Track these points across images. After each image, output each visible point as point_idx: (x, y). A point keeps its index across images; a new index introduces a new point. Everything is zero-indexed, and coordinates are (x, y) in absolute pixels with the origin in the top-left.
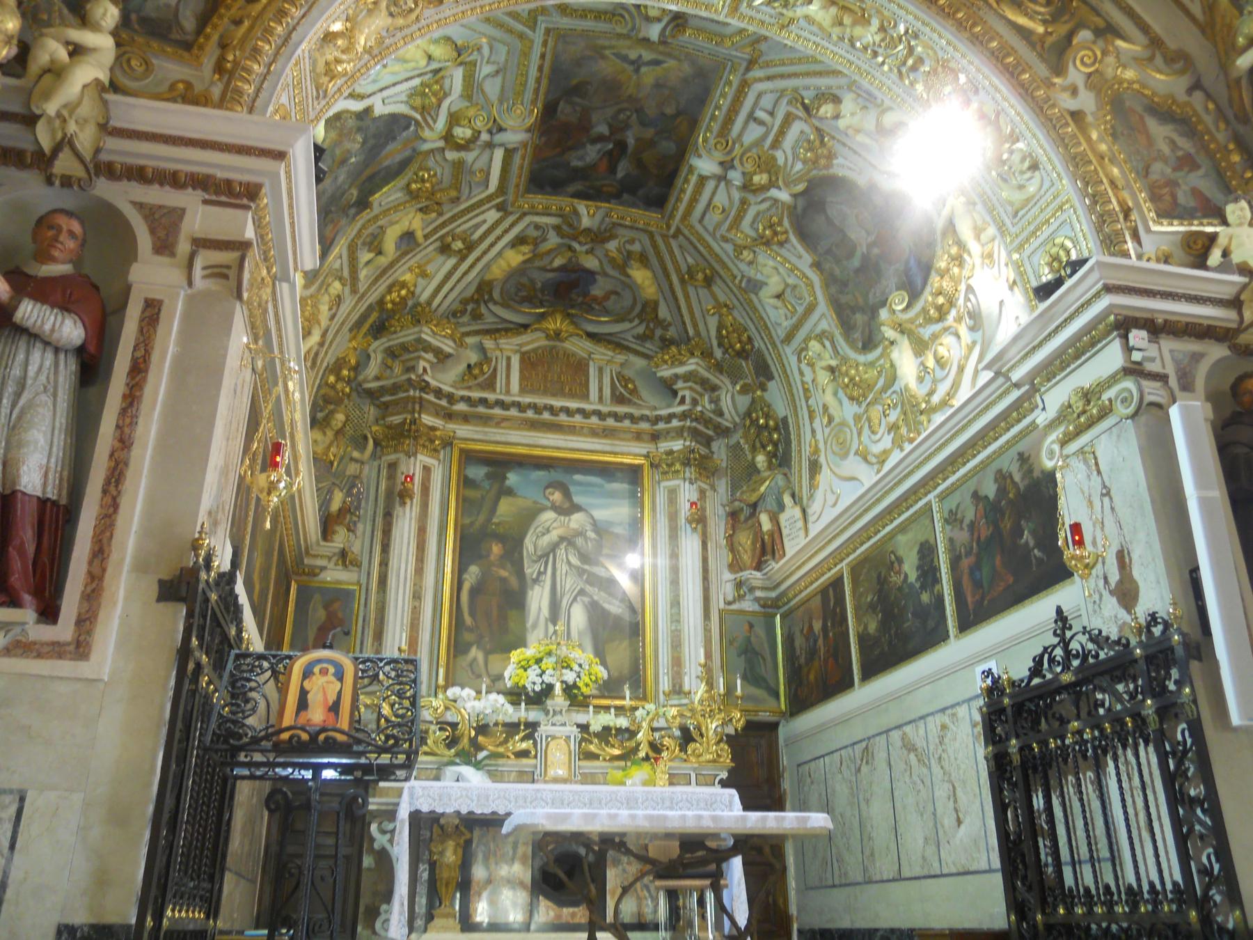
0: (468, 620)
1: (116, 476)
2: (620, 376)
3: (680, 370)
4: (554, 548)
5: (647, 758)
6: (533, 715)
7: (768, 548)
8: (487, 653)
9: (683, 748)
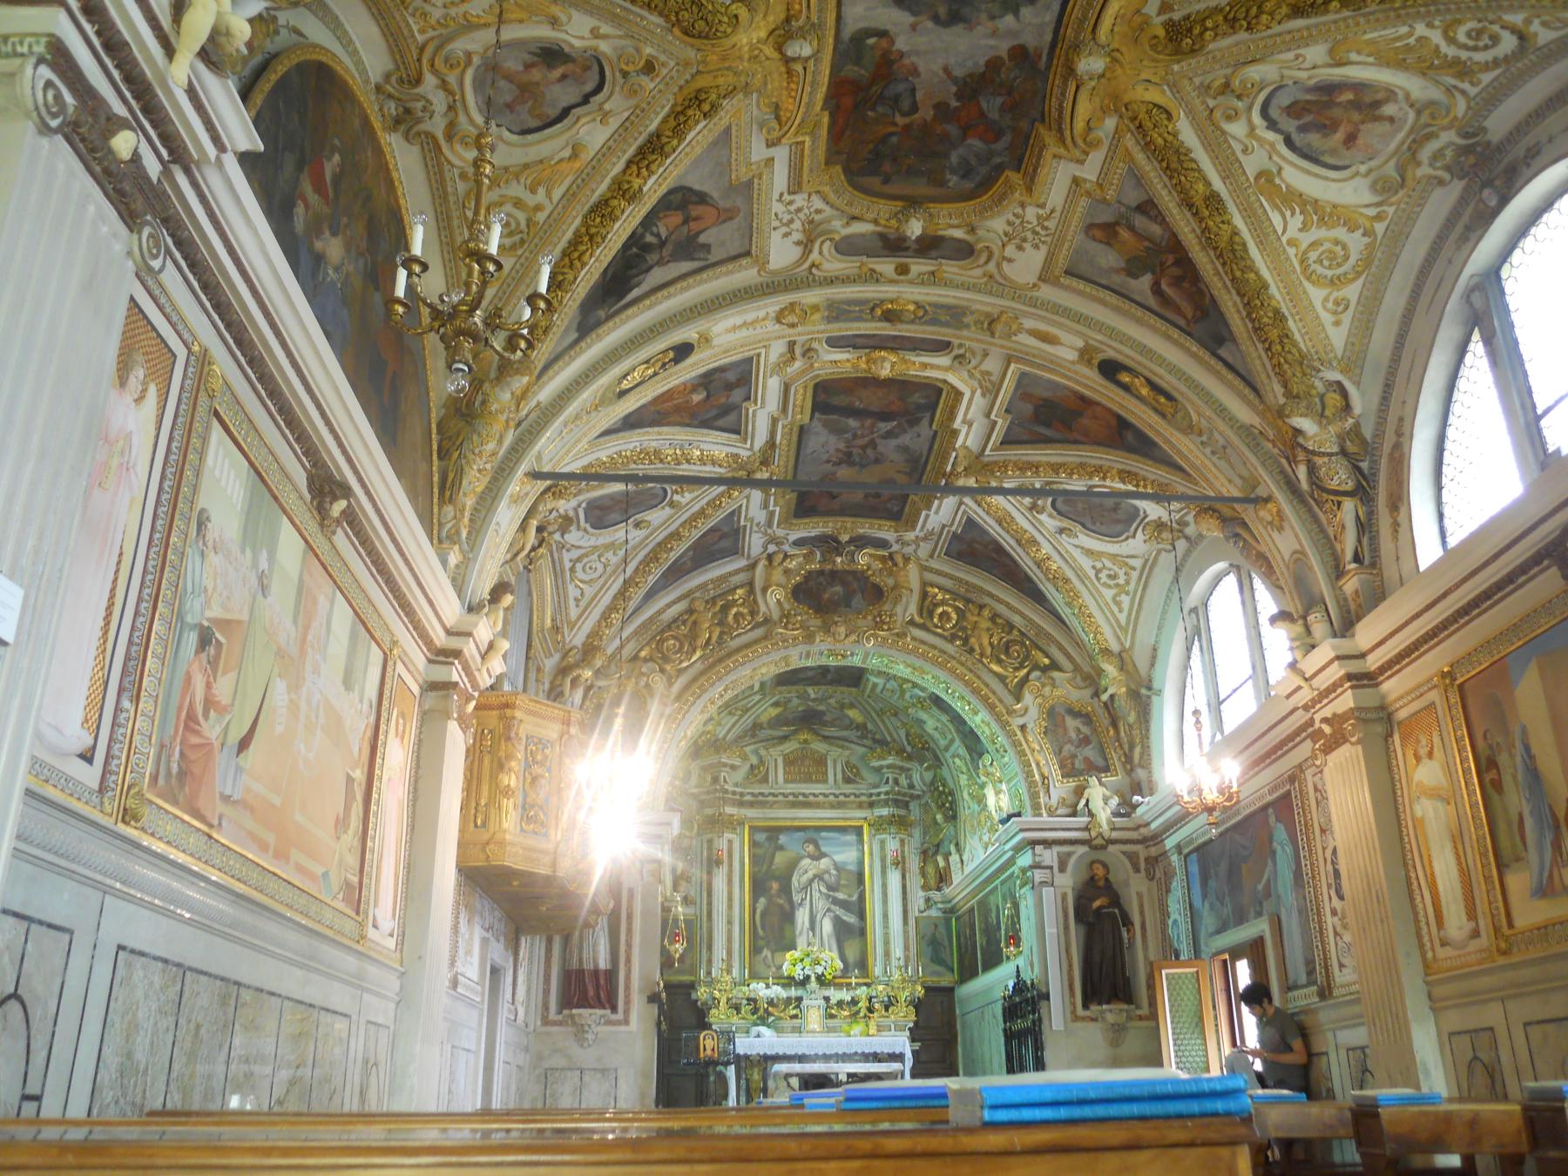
0: (761, 932)
1: (628, 961)
2: (847, 763)
3: (884, 763)
4: (811, 881)
5: (865, 1016)
6: (800, 992)
7: (943, 878)
8: (773, 952)
9: (887, 1009)
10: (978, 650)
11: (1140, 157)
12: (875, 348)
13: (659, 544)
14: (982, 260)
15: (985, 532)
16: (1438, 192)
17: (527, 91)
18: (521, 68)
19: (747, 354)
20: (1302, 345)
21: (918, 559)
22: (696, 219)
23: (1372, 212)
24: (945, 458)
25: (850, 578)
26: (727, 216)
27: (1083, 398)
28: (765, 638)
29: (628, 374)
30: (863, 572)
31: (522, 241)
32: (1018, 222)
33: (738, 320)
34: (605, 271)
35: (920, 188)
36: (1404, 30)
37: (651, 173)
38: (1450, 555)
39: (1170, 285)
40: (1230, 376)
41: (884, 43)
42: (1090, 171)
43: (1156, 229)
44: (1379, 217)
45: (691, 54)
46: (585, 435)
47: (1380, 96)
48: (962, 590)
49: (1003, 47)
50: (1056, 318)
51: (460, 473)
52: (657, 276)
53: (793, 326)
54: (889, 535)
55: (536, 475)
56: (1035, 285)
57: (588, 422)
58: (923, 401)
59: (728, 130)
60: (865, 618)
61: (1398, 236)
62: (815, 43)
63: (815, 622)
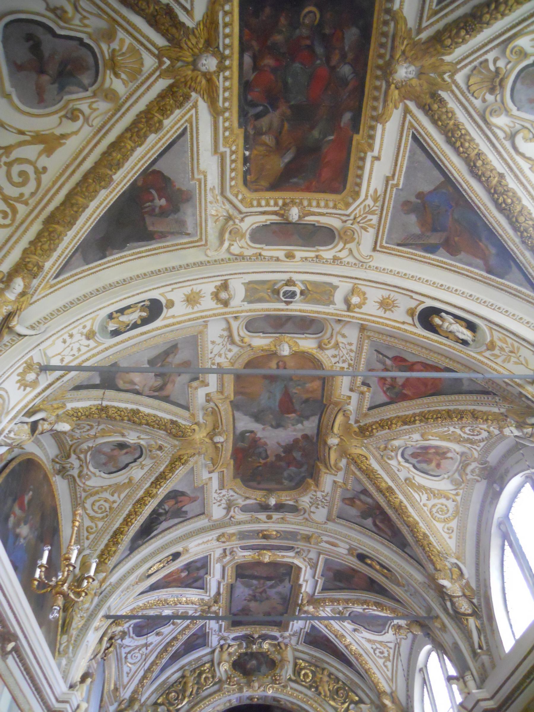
10: (323, 694)
11: (358, 473)
12: (261, 549)
13: (168, 643)
14: (302, 513)
15: (320, 632)
16: (478, 485)
17: (111, 458)
18: (109, 451)
19: (205, 555)
20: (437, 547)
21: (291, 645)
22: (181, 502)
23: (454, 492)
24: (298, 596)
25: (260, 656)
26: (193, 500)
27: (353, 569)
28: (219, 690)
29: (151, 567)
30: (266, 652)
31: (107, 515)
32: (314, 497)
33: (200, 541)
34: (142, 525)
35: (273, 486)
36: (446, 429)
37: (161, 487)
38: (519, 643)
39: (380, 522)
40: (412, 561)
41: (253, 435)
42: (339, 478)
43: (369, 500)
44: (457, 494)
45: (177, 443)
46: (132, 596)
47: (445, 450)
48: (314, 661)
49: (299, 435)
50: (336, 536)
51: (72, 618)
52: (164, 525)
53: (224, 542)
54: (277, 634)
55: (107, 617)
56: (325, 522)
57: (133, 589)
58: (285, 571)
59: (193, 468)
60: (267, 677)
61: (466, 500)
62: (225, 437)
63: (243, 681)
